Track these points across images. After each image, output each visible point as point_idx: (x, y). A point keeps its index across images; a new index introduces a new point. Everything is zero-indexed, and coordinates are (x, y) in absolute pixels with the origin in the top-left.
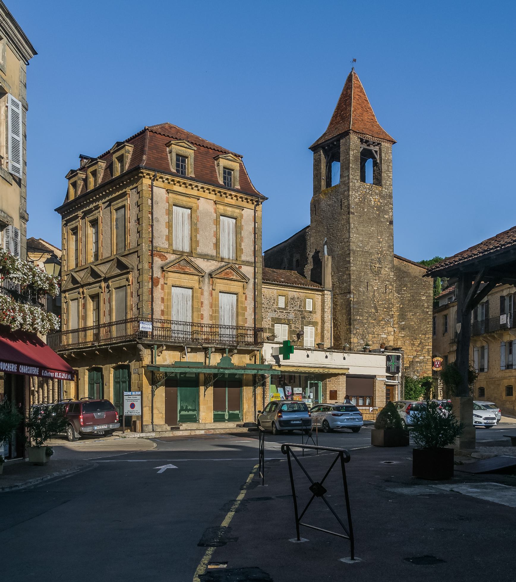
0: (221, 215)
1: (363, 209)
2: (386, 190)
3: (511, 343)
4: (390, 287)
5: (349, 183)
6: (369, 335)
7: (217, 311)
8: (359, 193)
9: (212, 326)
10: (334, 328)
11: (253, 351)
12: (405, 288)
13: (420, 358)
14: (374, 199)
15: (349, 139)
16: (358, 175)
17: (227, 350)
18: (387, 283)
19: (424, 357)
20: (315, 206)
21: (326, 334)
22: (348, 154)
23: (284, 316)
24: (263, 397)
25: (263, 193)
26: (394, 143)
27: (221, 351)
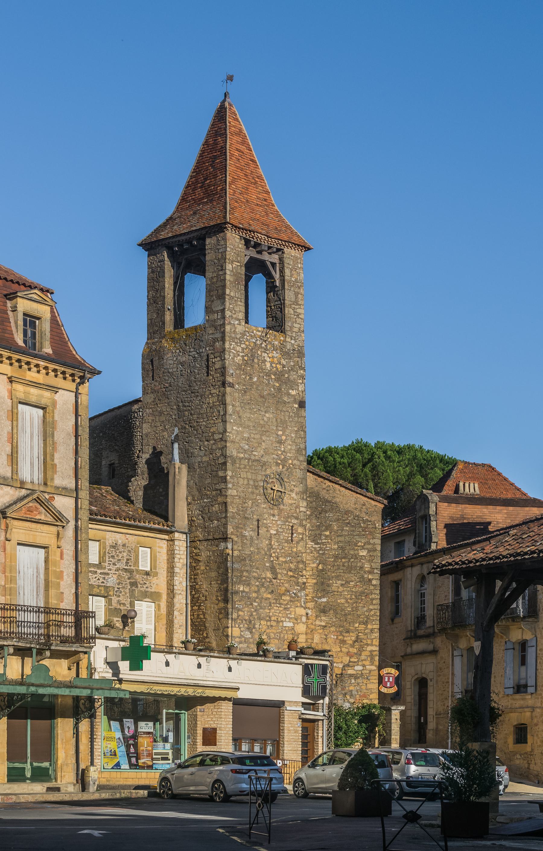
0: (20, 403)
1: (250, 378)
2: (293, 342)
3: (523, 645)
4: (300, 530)
5: (224, 325)
6: (262, 622)
7: (13, 580)
8: (243, 346)
9: (4, 607)
10: (192, 607)
11: (76, 653)
12: (327, 533)
13: (357, 668)
14: (270, 358)
15: (225, 239)
16: (240, 311)
17: (34, 651)
18: (294, 521)
19: (364, 666)
20: (152, 361)
21: (178, 618)
22: (223, 268)
23: (99, 579)
24: (91, 738)
25: (91, 361)
26: (308, 249)
27: (20, 652)
